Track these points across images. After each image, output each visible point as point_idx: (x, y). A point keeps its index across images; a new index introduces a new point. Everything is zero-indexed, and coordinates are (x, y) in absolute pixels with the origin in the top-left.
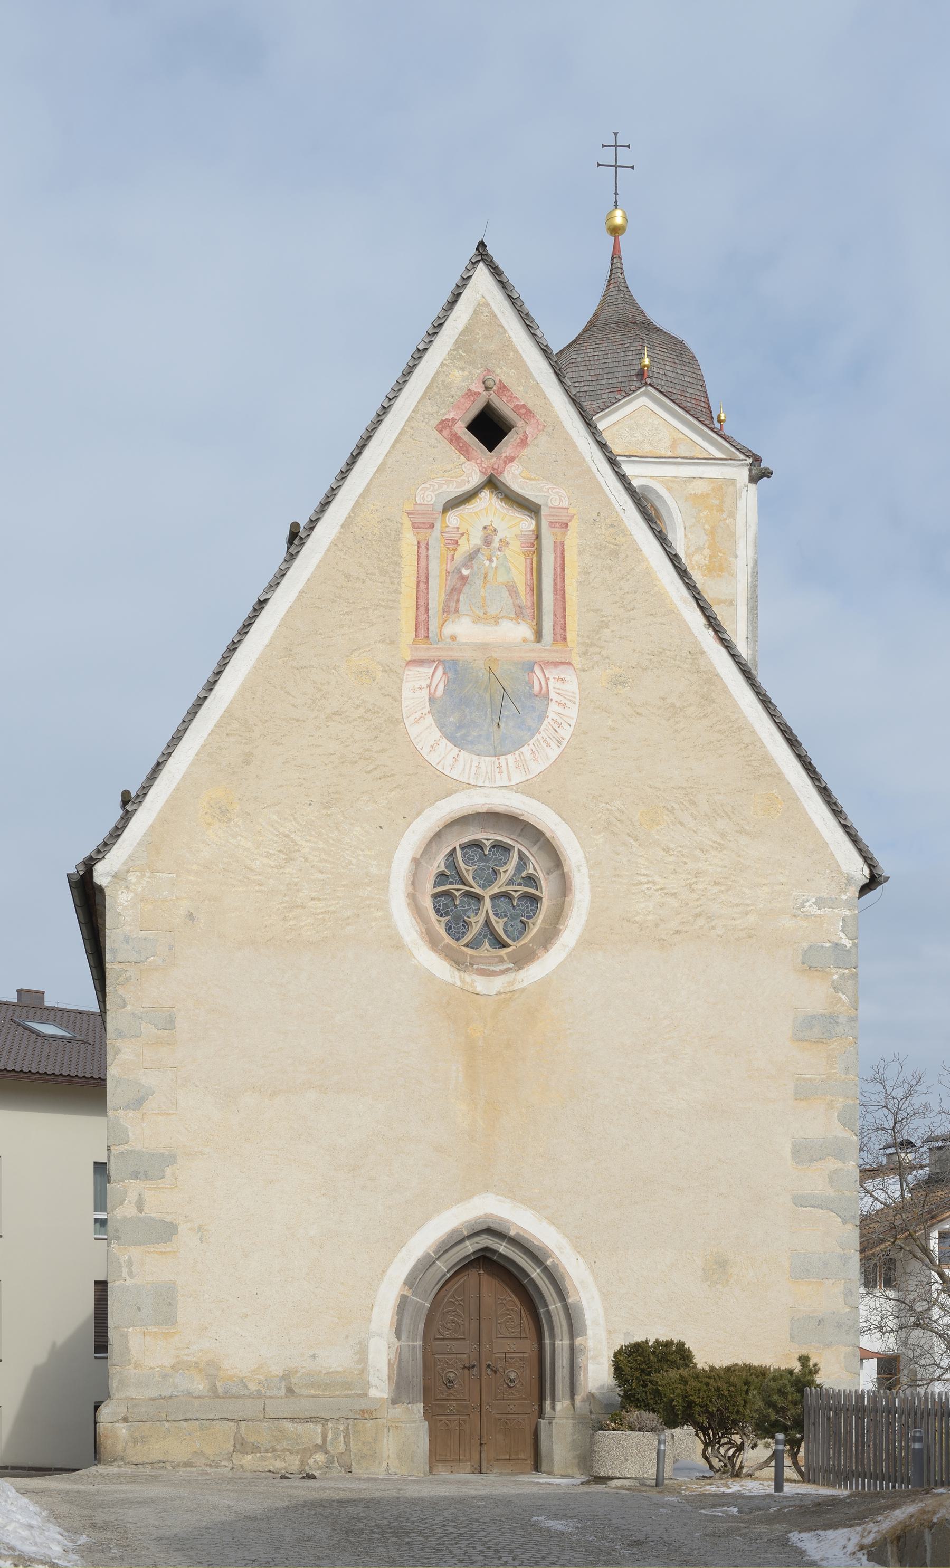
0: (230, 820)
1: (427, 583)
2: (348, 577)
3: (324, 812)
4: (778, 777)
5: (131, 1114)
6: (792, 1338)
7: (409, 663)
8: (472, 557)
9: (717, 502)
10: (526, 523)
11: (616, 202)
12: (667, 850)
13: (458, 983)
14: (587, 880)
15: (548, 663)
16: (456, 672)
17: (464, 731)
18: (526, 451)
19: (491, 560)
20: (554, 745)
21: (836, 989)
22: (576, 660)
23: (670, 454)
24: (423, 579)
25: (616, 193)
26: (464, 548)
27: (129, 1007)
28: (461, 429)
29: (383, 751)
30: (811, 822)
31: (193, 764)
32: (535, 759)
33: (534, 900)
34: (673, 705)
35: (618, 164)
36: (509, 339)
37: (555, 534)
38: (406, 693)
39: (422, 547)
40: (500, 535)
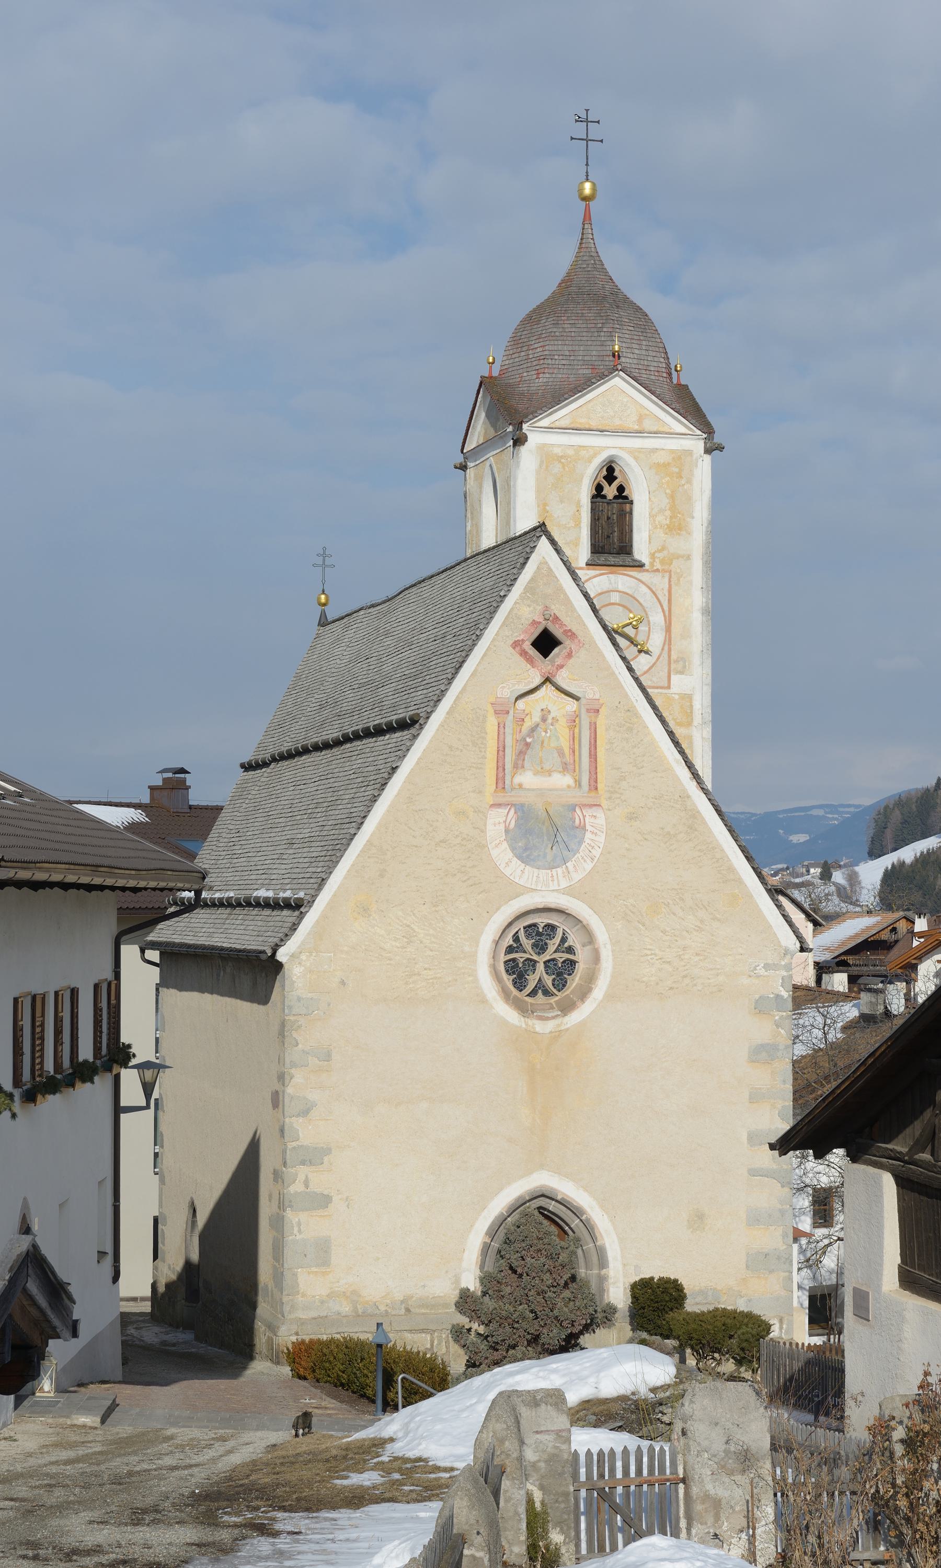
0: (370, 915)
1: (504, 751)
2: (451, 747)
3: (433, 909)
4: (740, 881)
5: (301, 1120)
6: (747, 1267)
7: (492, 806)
8: (533, 730)
9: (677, 470)
10: (571, 705)
11: (587, 172)
12: (664, 932)
13: (524, 1026)
14: (610, 953)
15: (585, 805)
16: (524, 812)
17: (528, 853)
18: (571, 661)
19: (546, 732)
20: (588, 861)
21: (778, 1026)
22: (605, 804)
23: (636, 427)
24: (501, 749)
25: (587, 165)
26: (528, 724)
27: (300, 1046)
28: (527, 646)
29: (474, 866)
30: (760, 911)
31: (345, 878)
32: (576, 871)
33: (572, 963)
34: (669, 833)
35: (589, 138)
36: (561, 585)
37: (590, 717)
38: (490, 827)
39: (501, 726)
40: (553, 714)
